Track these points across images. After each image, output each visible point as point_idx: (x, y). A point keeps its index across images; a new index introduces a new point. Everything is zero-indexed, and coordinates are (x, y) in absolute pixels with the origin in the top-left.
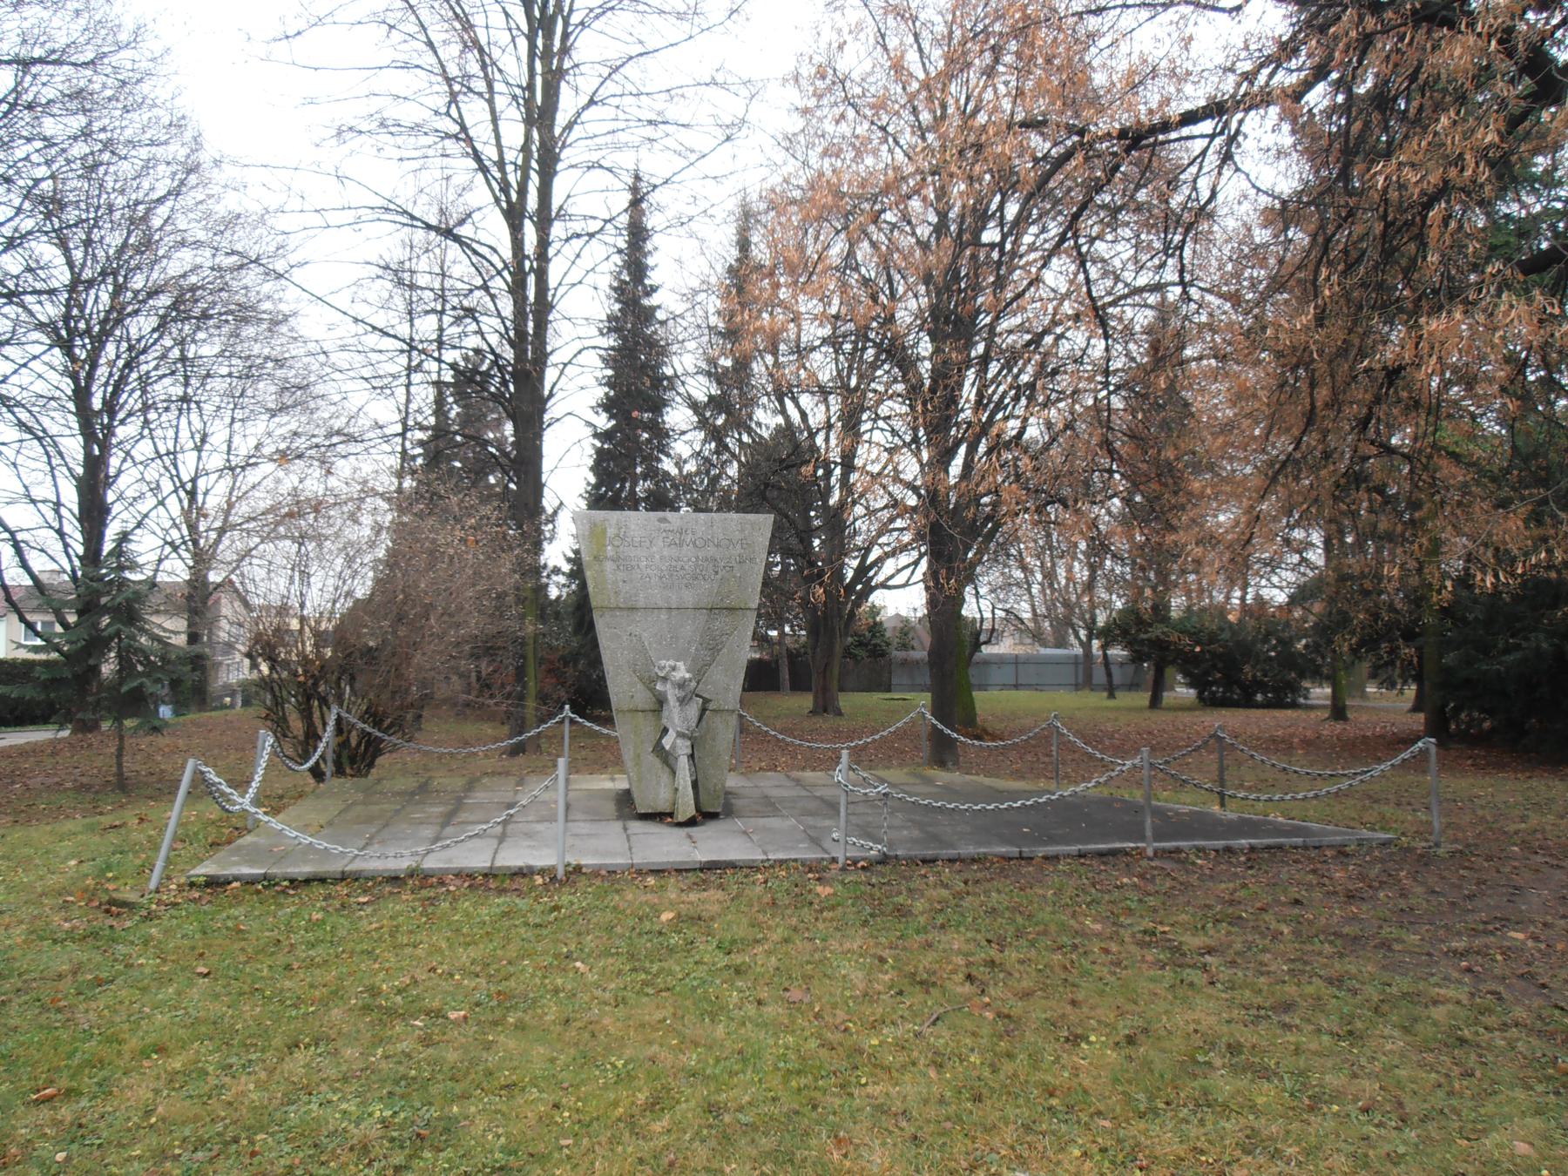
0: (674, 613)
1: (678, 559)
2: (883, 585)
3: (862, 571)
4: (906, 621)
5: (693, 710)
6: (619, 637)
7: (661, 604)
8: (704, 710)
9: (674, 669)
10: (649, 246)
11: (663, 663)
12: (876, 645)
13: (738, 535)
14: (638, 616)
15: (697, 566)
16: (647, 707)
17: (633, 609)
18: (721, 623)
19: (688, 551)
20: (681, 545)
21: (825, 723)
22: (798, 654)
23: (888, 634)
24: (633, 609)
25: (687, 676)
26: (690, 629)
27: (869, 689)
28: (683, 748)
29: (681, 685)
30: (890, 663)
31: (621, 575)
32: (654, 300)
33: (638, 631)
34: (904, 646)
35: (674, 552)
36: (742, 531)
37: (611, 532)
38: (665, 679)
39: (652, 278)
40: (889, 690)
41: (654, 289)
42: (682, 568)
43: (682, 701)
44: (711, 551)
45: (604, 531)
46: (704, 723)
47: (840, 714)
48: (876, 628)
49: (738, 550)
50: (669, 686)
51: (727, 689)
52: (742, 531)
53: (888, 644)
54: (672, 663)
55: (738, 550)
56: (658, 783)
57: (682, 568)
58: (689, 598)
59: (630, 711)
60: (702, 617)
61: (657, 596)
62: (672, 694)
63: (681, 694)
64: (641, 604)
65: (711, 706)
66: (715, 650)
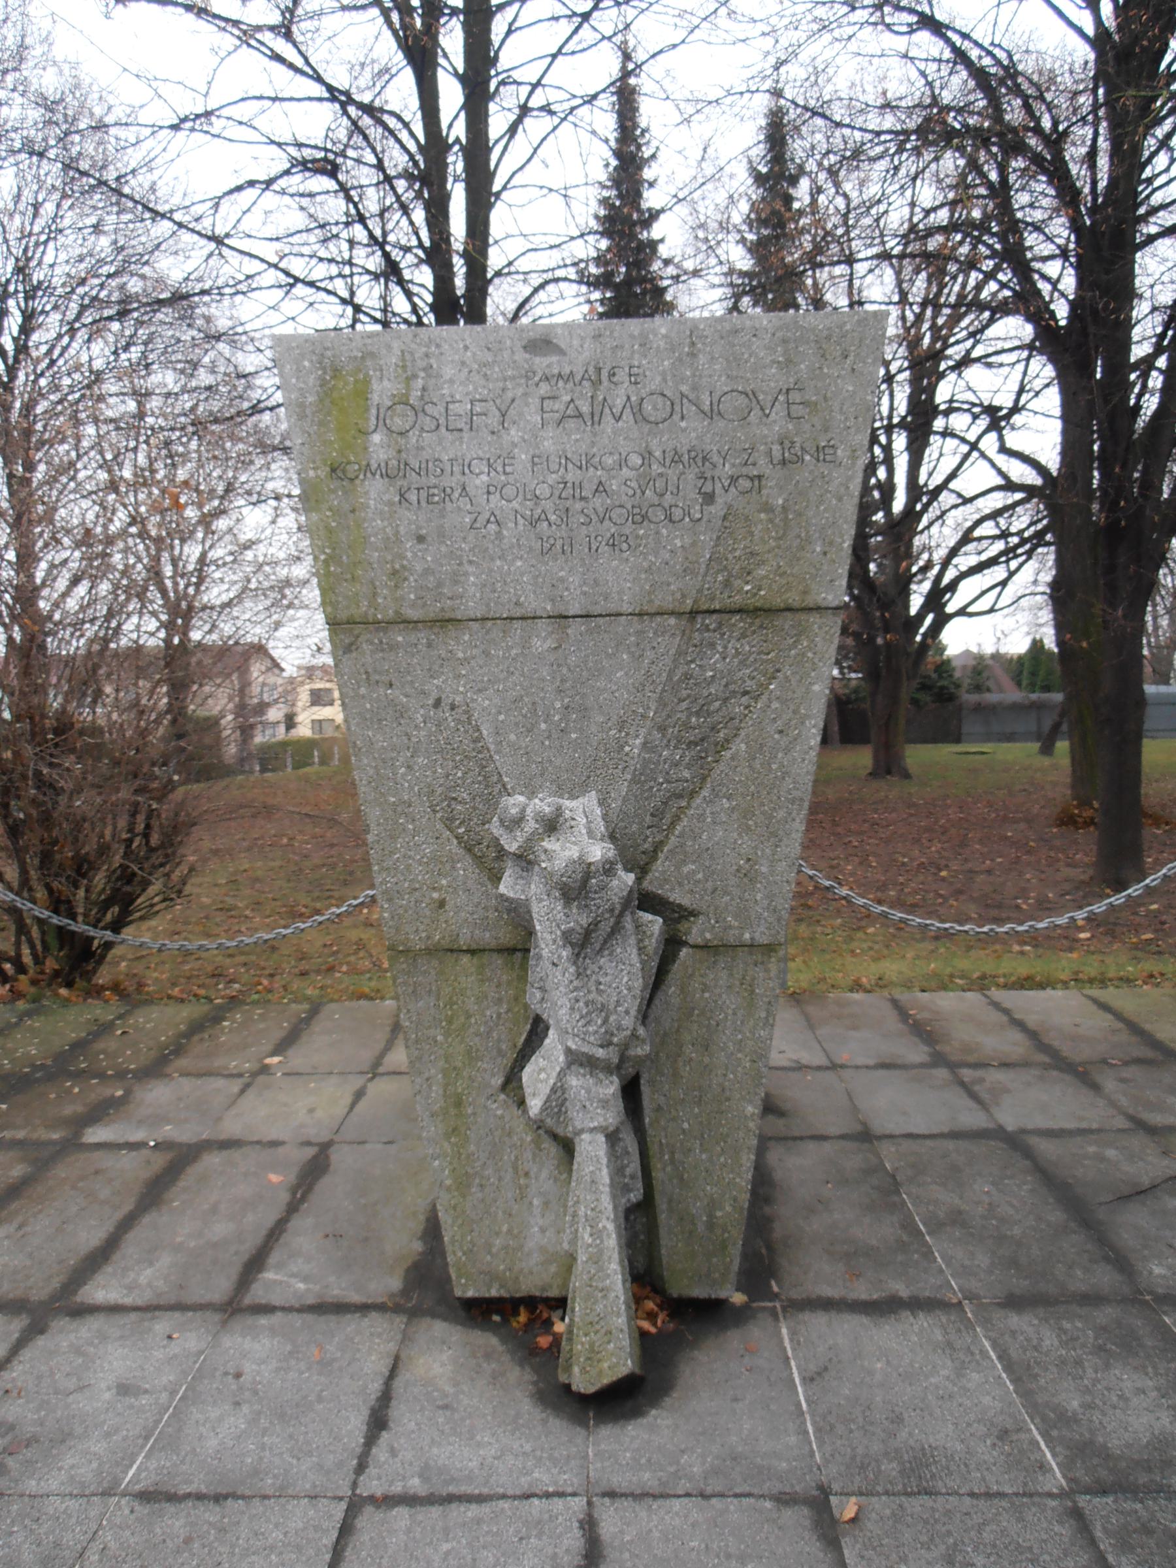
0: (576, 628)
1: (588, 462)
2: (962, 612)
3: (935, 600)
4: (980, 658)
5: (623, 973)
6: (401, 713)
7: (533, 603)
8: (672, 944)
9: (552, 825)
10: (647, 174)
11: (514, 803)
12: (942, 688)
13: (773, 379)
14: (461, 644)
15: (646, 480)
16: (487, 938)
17: (445, 622)
18: (727, 655)
19: (618, 437)
20: (595, 418)
21: (890, 789)
22: (848, 701)
23: (957, 674)
24: (445, 622)
25: (598, 852)
26: (623, 679)
27: (934, 740)
28: (595, 1106)
29: (576, 888)
30: (960, 708)
31: (408, 519)
32: (657, 231)
33: (457, 690)
34: (978, 688)
35: (576, 439)
36: (789, 363)
37: (382, 390)
38: (526, 860)
39: (651, 199)
40: (958, 740)
41: (654, 215)
42: (600, 488)
43: (584, 944)
44: (691, 431)
45: (362, 392)
46: (671, 989)
47: (906, 775)
48: (944, 667)
49: (778, 423)
50: (536, 888)
51: (748, 876)
52: (789, 363)
53: (958, 686)
54: (542, 804)
55: (778, 423)
56: (522, 1195)
57: (600, 488)
58: (621, 581)
59: (432, 951)
60: (665, 641)
61: (523, 582)
62: (550, 921)
63: (580, 919)
64: (471, 606)
65: (696, 932)
66: (706, 746)
